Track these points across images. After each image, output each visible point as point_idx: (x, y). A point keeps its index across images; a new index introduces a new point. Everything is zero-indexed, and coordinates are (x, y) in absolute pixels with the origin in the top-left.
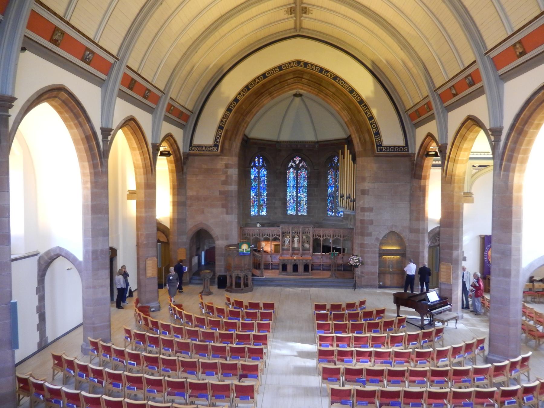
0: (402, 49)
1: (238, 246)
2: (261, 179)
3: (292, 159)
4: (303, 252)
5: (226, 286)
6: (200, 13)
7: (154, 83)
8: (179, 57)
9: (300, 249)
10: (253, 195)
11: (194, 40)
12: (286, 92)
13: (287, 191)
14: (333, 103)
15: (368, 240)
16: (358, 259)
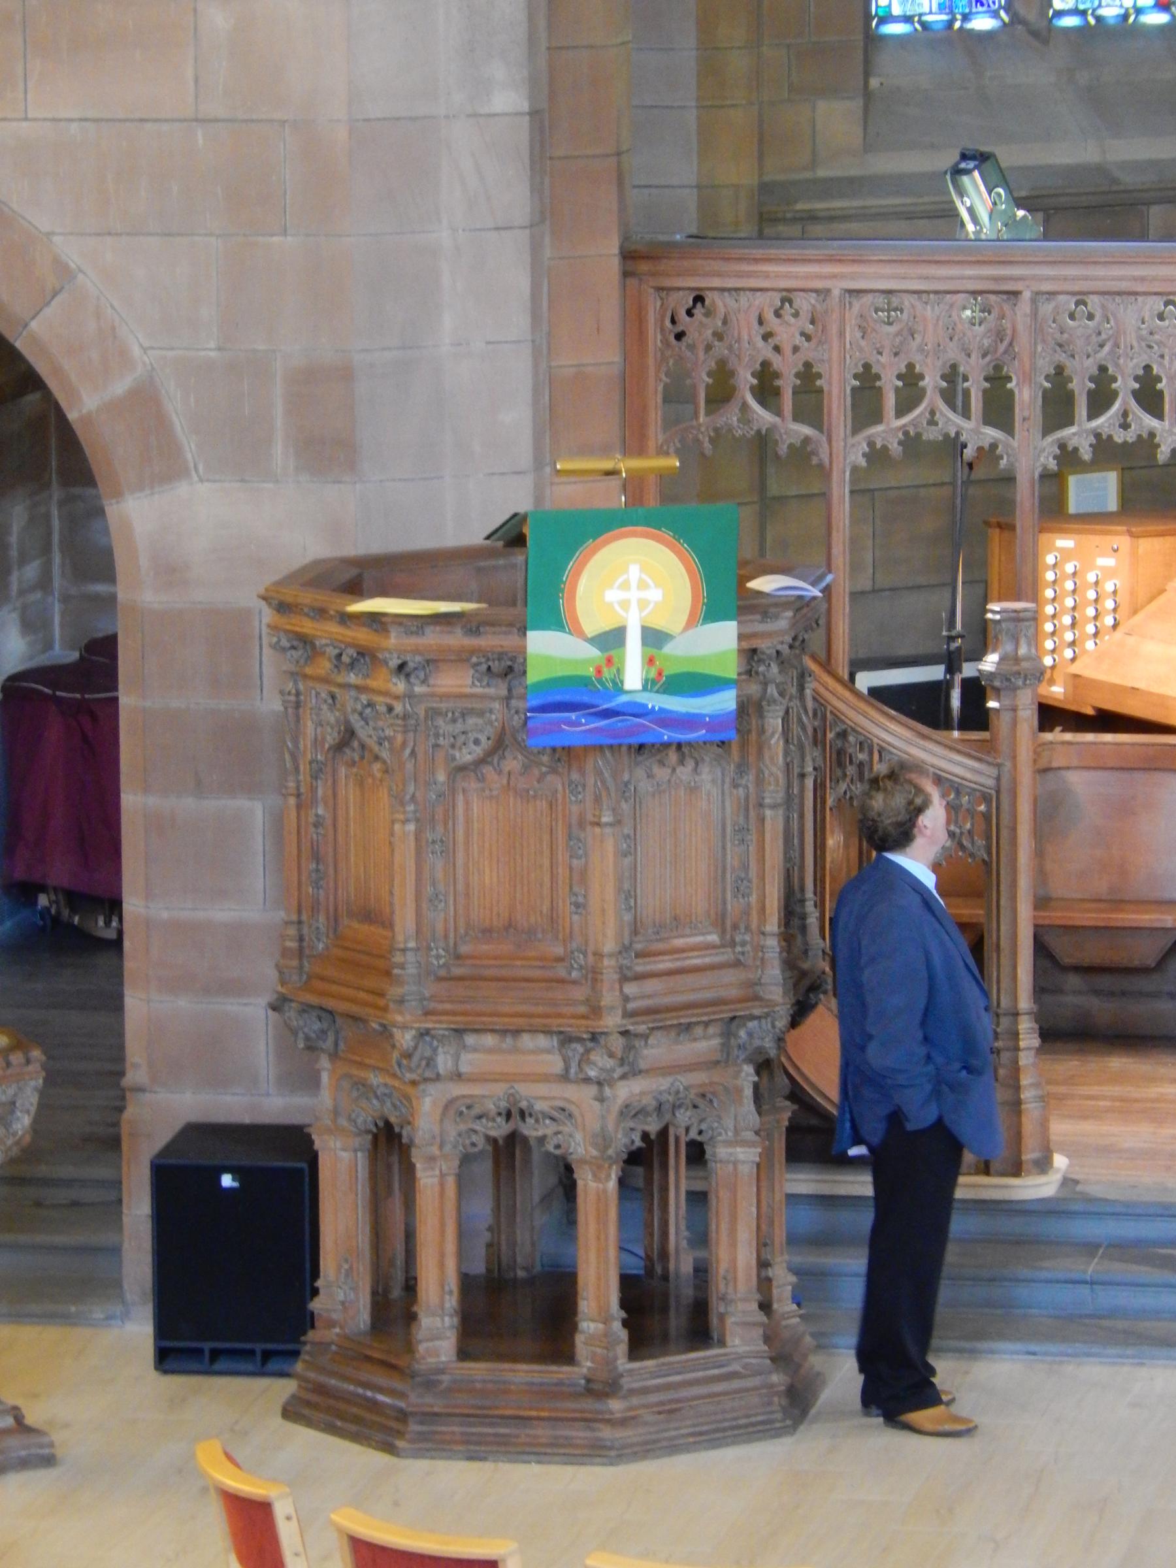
5: (308, 1321)
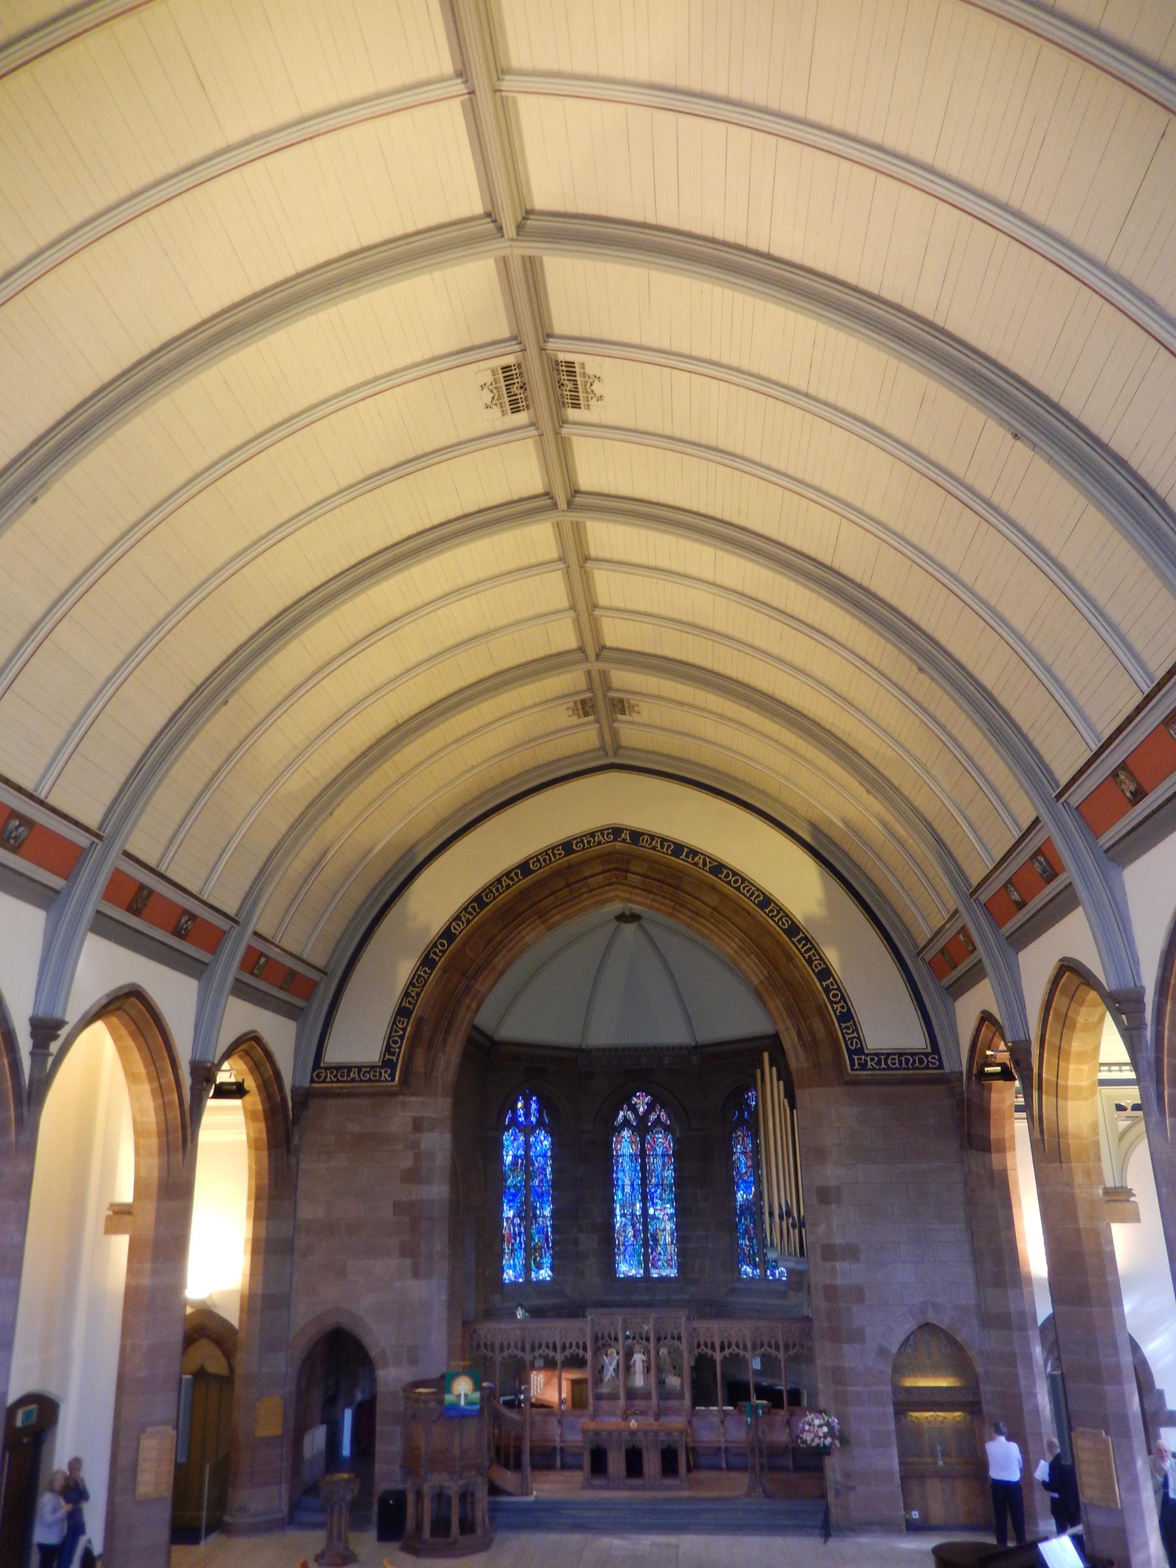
0: (868, 792)
1: (443, 1383)
2: (533, 1165)
3: (625, 1100)
4: (662, 1403)
6: (337, 720)
7: (206, 896)
8: (284, 828)
9: (650, 1393)
10: (511, 1214)
11: (323, 785)
12: (584, 909)
13: (614, 1201)
14: (716, 935)
15: (853, 1357)
16: (828, 1424)
